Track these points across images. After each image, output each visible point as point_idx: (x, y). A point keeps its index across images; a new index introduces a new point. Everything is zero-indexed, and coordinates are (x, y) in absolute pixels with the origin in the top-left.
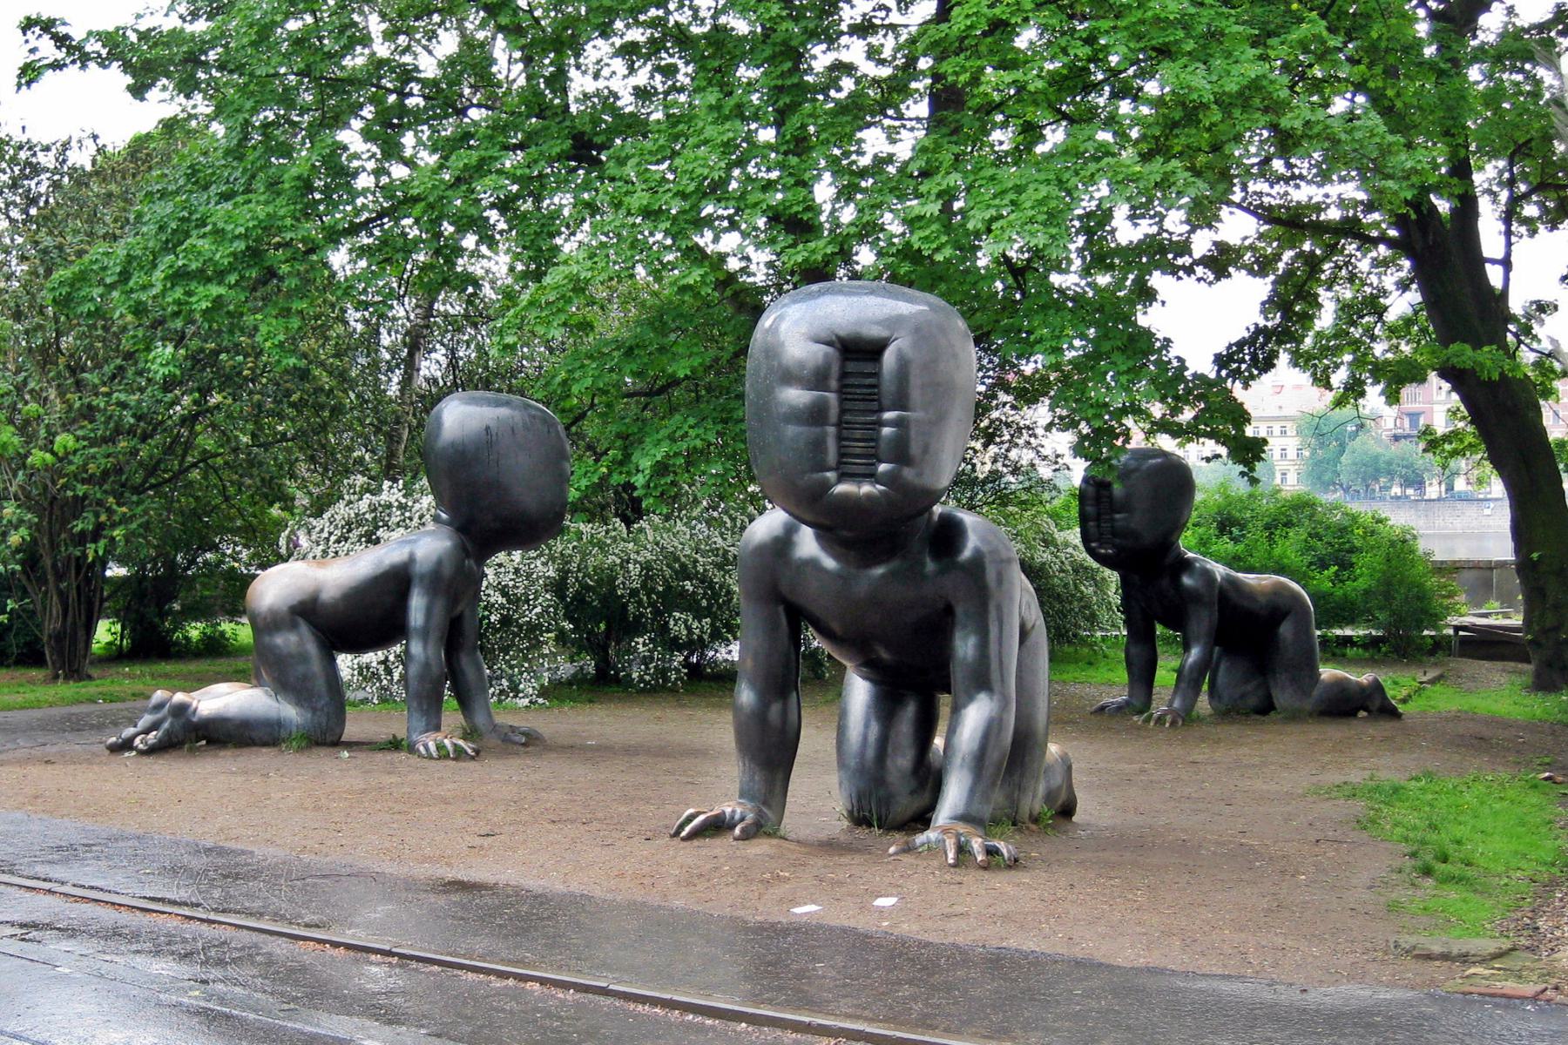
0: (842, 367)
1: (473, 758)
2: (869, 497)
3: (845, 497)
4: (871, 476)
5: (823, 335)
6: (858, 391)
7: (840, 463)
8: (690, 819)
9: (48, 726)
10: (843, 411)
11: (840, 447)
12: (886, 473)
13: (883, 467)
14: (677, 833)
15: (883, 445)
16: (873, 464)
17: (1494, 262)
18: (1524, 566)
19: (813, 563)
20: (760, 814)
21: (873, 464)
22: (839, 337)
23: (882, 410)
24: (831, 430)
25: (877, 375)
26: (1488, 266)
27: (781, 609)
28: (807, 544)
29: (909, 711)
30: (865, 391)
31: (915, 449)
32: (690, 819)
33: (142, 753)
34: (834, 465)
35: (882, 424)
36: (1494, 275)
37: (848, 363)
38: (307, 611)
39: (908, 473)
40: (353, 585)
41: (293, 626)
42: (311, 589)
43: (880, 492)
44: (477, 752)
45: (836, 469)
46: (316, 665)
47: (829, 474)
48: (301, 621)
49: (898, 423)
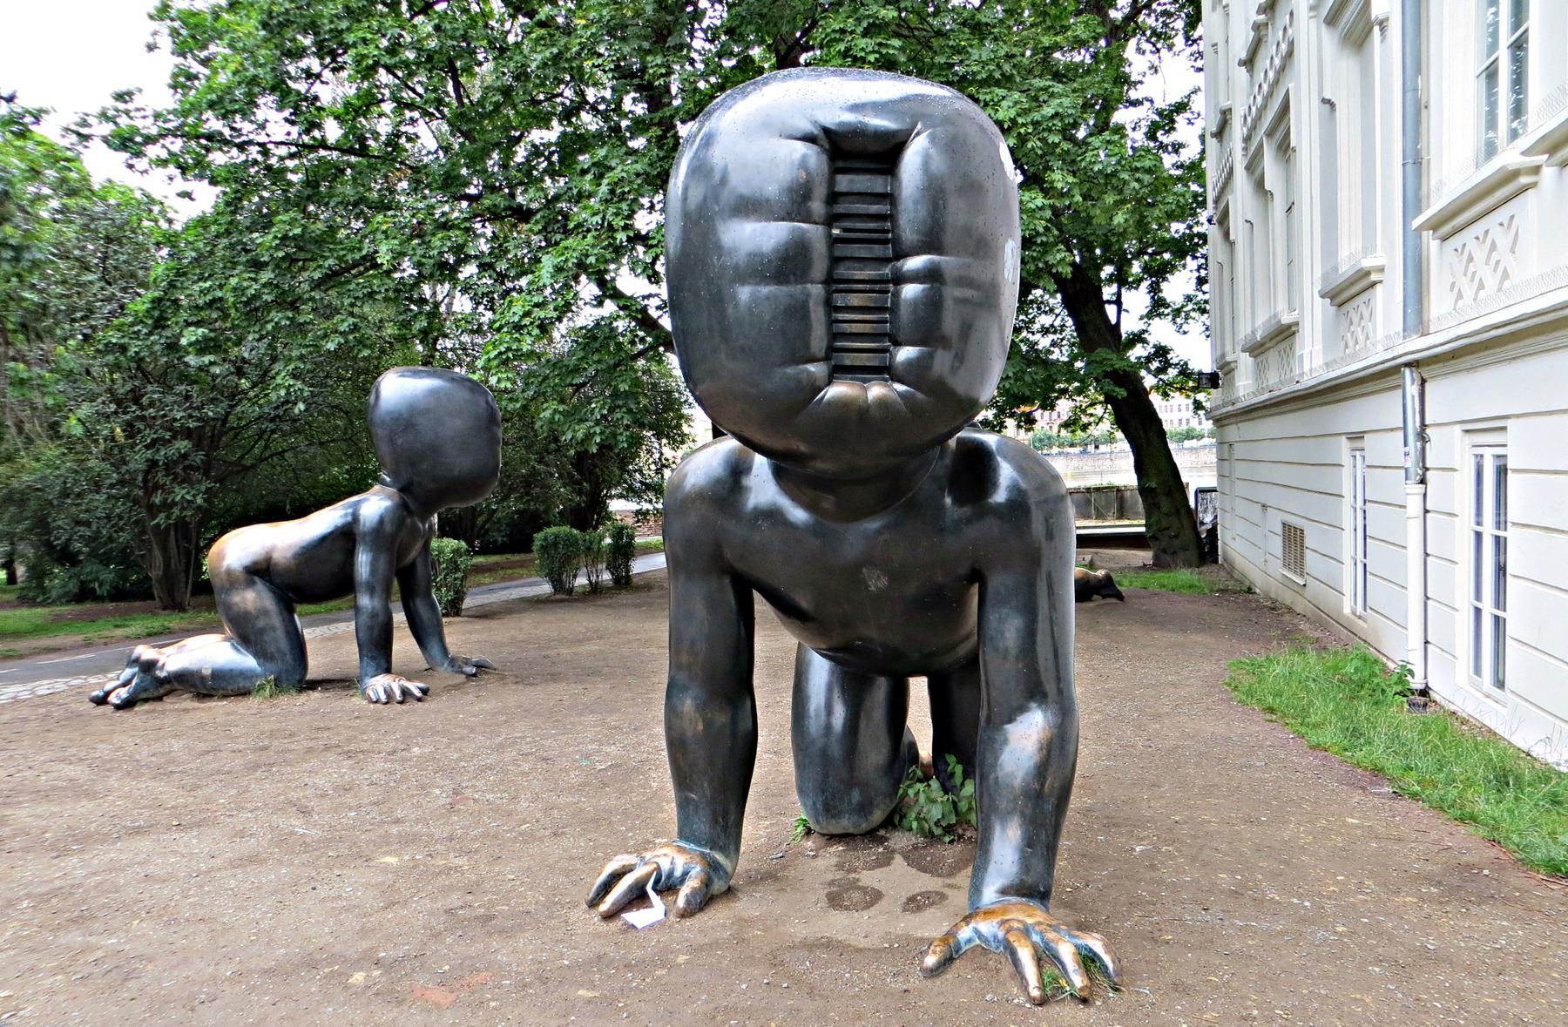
0: (831, 182)
1: (419, 700)
2: (882, 403)
3: (842, 405)
4: (885, 371)
5: (806, 127)
6: (860, 225)
7: (831, 350)
8: (616, 877)
9: (1342, 291)
10: (835, 261)
11: (832, 322)
12: (910, 363)
13: (905, 353)
14: (593, 904)
15: (905, 313)
16: (885, 350)
17: (1109, 302)
18: (1143, 490)
19: (772, 515)
20: (713, 867)
21: (885, 350)
22: (826, 131)
23: (901, 255)
24: (817, 290)
25: (890, 198)
26: (1107, 306)
27: (727, 581)
28: (762, 486)
29: (881, 687)
30: (872, 225)
31: (950, 323)
32: (616, 877)
33: (118, 707)
34: (822, 354)
35: (900, 279)
36: (1111, 311)
37: (840, 177)
38: (260, 571)
39: (942, 362)
40: (304, 544)
41: (250, 584)
42: (263, 552)
43: (900, 394)
44: (425, 692)
45: (827, 358)
46: (276, 620)
47: (811, 368)
48: (256, 579)
49: (931, 276)
